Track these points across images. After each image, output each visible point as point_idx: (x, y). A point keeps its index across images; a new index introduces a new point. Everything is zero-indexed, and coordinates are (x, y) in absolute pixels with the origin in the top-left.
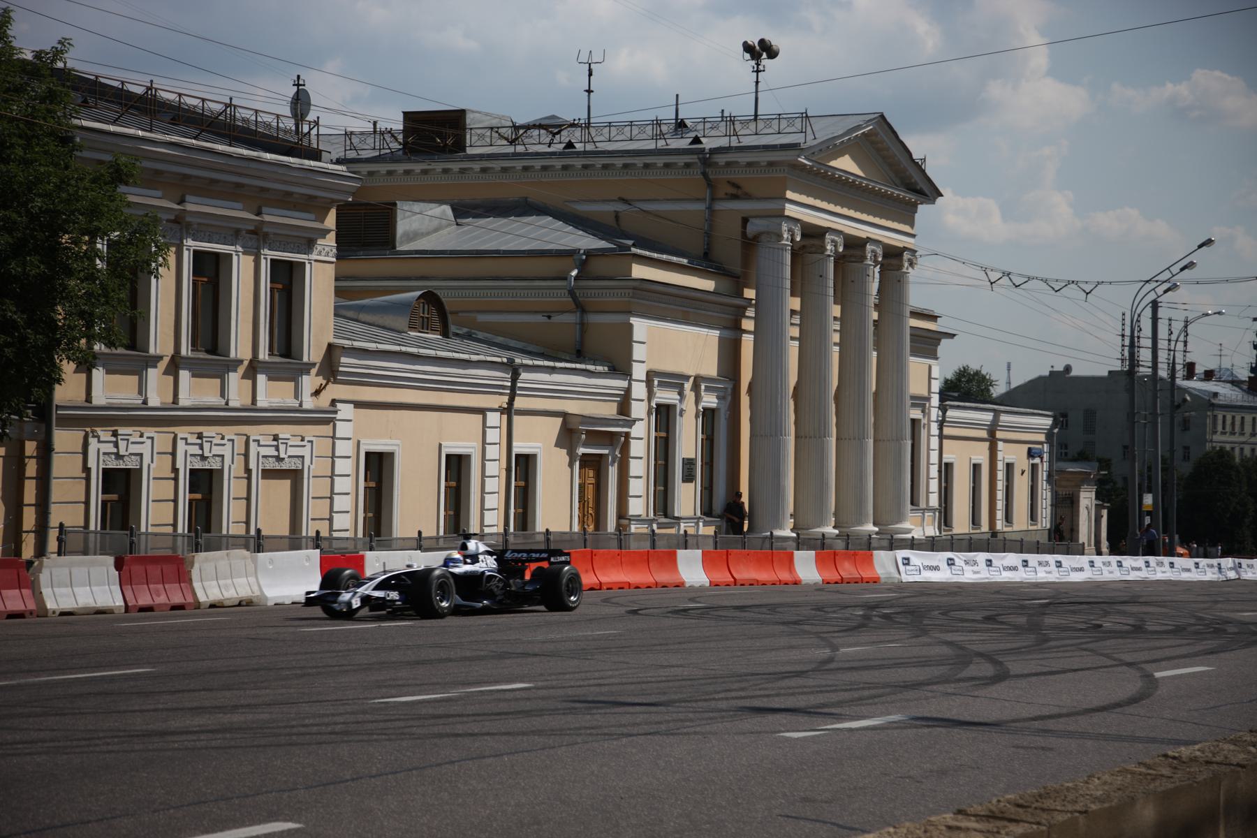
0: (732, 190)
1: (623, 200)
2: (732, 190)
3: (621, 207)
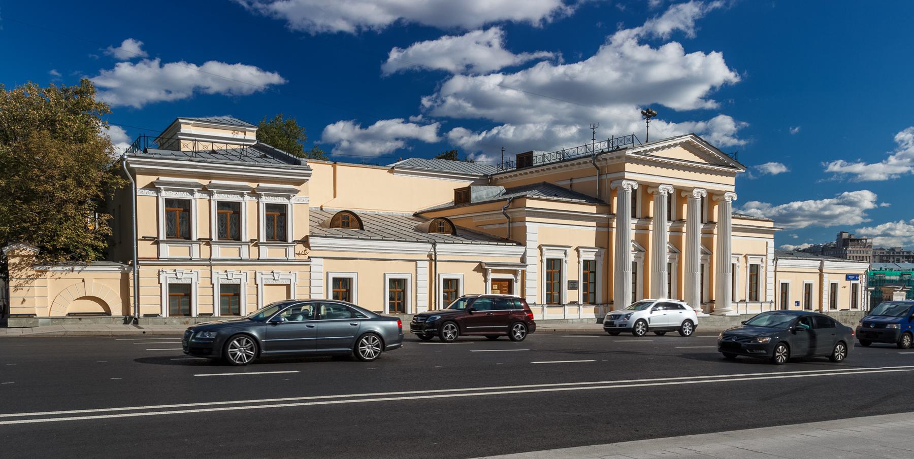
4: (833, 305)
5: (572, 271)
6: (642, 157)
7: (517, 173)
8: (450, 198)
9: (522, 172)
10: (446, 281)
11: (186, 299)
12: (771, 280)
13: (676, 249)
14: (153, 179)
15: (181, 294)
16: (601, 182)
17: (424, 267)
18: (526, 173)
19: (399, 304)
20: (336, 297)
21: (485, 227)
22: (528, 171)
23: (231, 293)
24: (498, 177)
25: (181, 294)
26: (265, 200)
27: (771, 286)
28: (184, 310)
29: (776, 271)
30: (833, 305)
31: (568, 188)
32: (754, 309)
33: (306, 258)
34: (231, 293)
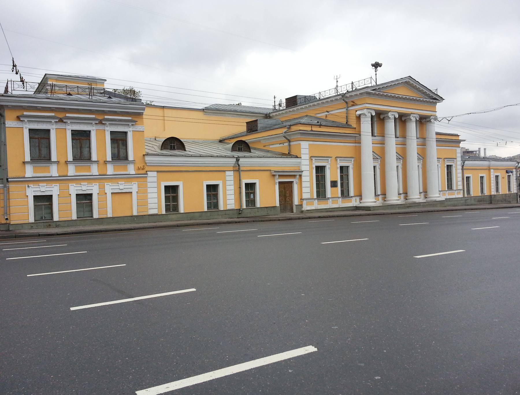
0: (353, 104)
1: (328, 112)
2: (353, 104)
3: (327, 113)
4: (497, 190)
5: (332, 174)
6: (377, 93)
7: (288, 110)
8: (244, 129)
9: (291, 110)
10: (247, 185)
11: (50, 206)
12: (460, 175)
13: (402, 156)
14: (19, 113)
15: (44, 201)
16: (347, 113)
17: (230, 175)
18: (294, 111)
19: (173, 196)
20: (35, 220)
21: (271, 146)
22: (295, 109)
23: (84, 199)
24: (274, 114)
25: (44, 201)
26: (109, 129)
27: (460, 179)
28: (470, 159)
29: (462, 169)
30: (497, 190)
31: (325, 118)
32: (448, 195)
33: (144, 172)
34: (84, 199)
